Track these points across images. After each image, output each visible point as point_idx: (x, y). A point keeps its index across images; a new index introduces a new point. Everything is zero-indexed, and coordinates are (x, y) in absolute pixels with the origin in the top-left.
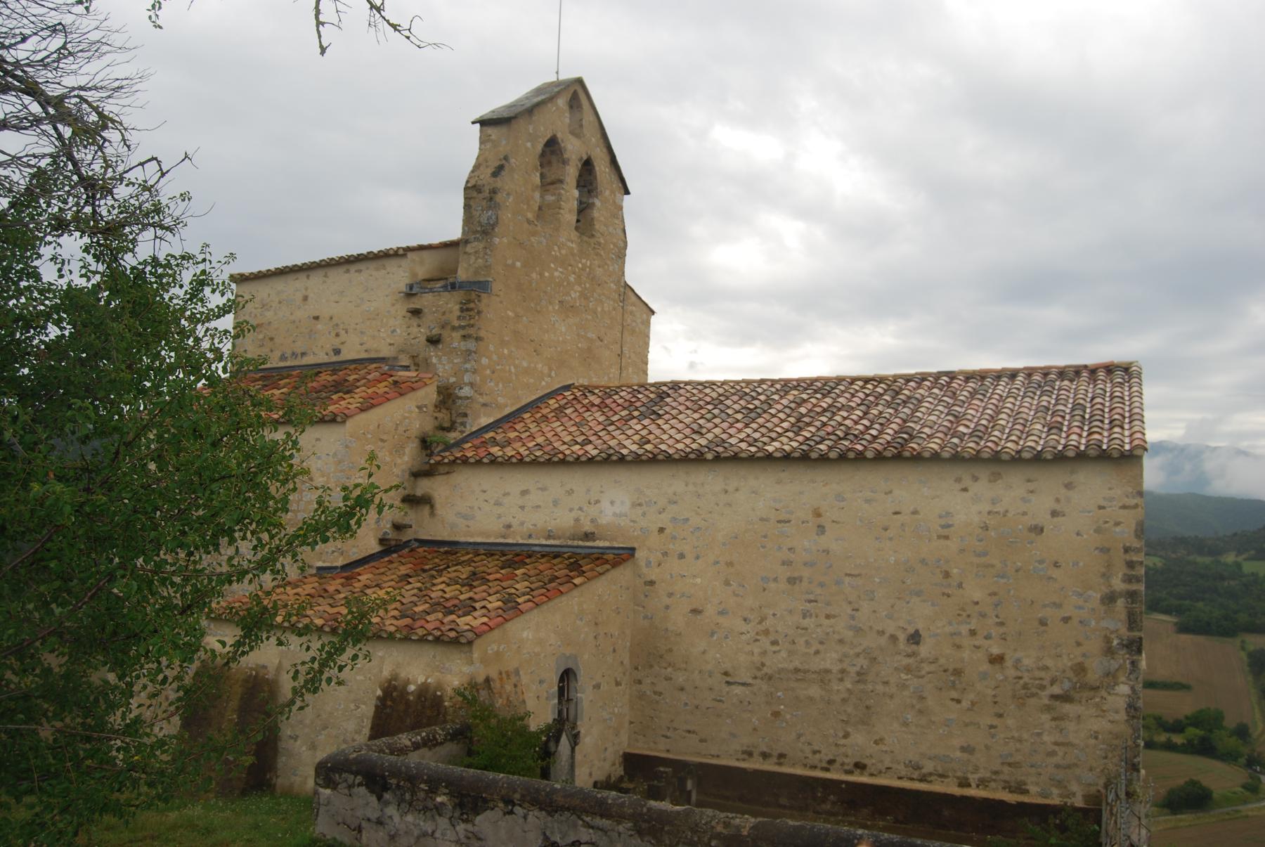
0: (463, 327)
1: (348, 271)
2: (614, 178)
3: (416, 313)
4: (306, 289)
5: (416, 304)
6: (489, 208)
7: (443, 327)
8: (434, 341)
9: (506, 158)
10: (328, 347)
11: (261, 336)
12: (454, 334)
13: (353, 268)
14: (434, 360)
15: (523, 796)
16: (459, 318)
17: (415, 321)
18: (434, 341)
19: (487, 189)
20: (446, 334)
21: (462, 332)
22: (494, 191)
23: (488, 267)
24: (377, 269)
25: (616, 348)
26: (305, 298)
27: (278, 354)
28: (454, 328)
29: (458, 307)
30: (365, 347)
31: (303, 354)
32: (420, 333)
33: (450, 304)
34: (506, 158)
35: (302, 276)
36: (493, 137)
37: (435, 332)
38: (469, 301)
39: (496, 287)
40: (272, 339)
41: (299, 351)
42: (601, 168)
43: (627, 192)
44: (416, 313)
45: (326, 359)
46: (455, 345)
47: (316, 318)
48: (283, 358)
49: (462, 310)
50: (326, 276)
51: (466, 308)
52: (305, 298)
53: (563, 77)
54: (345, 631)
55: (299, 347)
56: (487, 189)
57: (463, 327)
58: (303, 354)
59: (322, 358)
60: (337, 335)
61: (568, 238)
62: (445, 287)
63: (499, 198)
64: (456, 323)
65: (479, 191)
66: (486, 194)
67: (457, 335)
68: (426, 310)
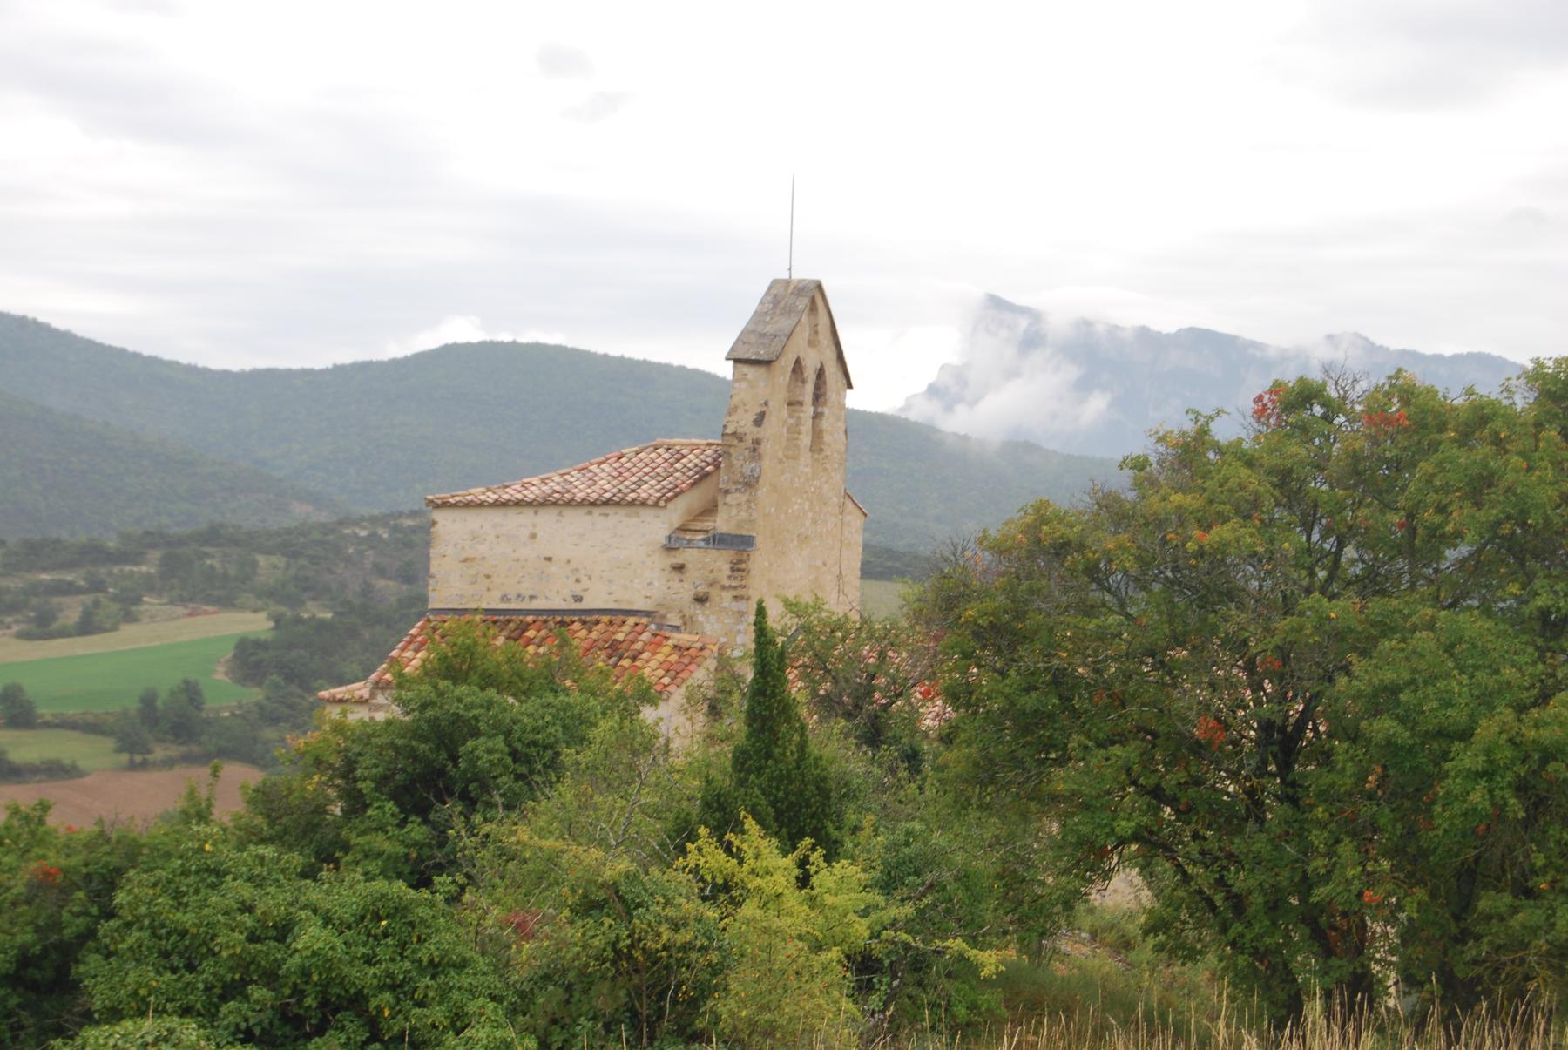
0: (735, 588)
1: (590, 513)
2: (840, 375)
3: (680, 568)
4: (534, 526)
5: (678, 559)
6: (753, 459)
7: (711, 585)
8: (701, 600)
9: (766, 404)
10: (566, 592)
11: (472, 572)
12: (724, 594)
13: (597, 511)
14: (700, 618)
15: (1373, 873)
16: (729, 577)
17: (676, 576)
18: (701, 600)
19: (749, 439)
20: (714, 592)
21: (735, 593)
22: (757, 442)
23: (752, 522)
24: (628, 516)
25: (836, 570)
26: (533, 536)
27: (497, 594)
28: (723, 588)
29: (728, 566)
30: (614, 597)
31: (532, 597)
32: (685, 590)
33: (720, 562)
34: (766, 404)
35: (529, 512)
36: (750, 377)
37: (702, 589)
38: (740, 562)
39: (759, 540)
40: (488, 577)
41: (527, 593)
42: (832, 371)
43: (850, 386)
44: (680, 568)
45: (564, 606)
46: (726, 604)
47: (549, 559)
48: (504, 598)
49: (732, 570)
50: (560, 514)
51: (738, 568)
52: (533, 536)
53: (796, 276)
54: (1321, 908)
55: (526, 589)
56: (749, 439)
57: (735, 588)
58: (532, 597)
59: (557, 603)
60: (578, 581)
61: (806, 457)
62: (706, 540)
63: (763, 448)
64: (727, 583)
65: (741, 440)
66: (749, 443)
67: (727, 595)
68: (689, 566)
